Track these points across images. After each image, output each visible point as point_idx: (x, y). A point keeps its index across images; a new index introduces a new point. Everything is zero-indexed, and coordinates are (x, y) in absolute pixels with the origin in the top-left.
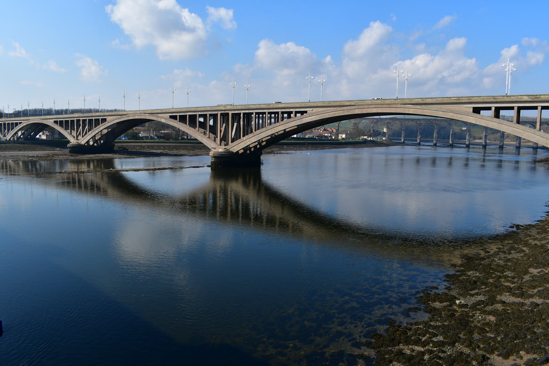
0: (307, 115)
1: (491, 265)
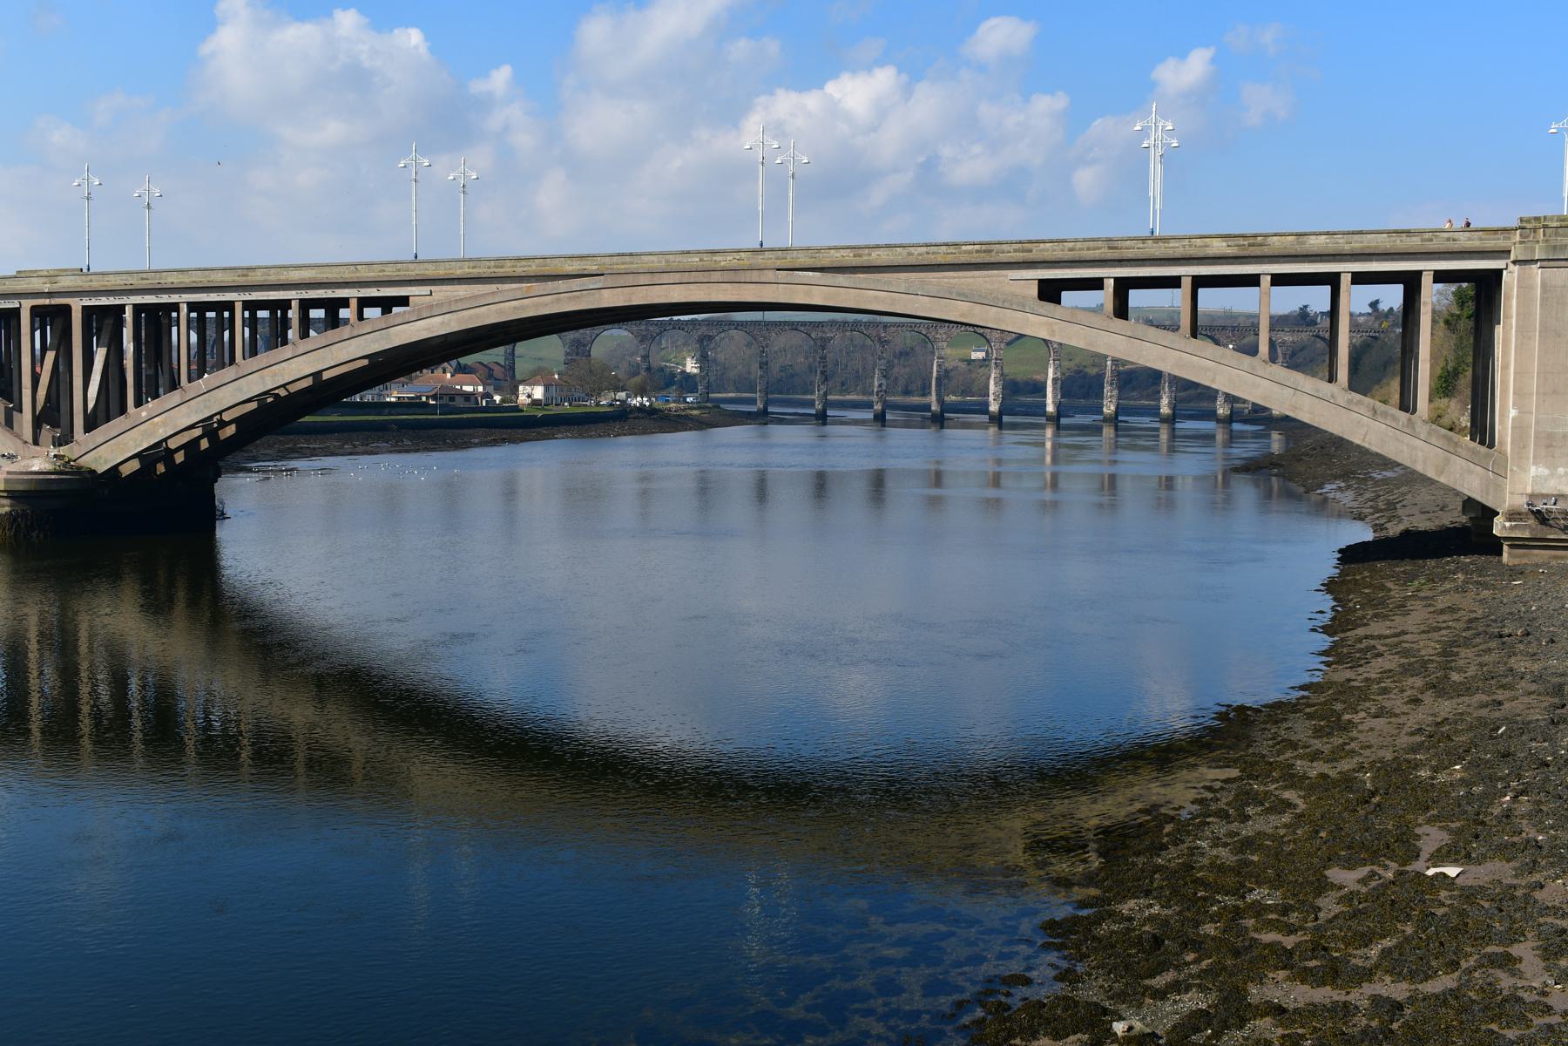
0: (409, 312)
1: (1193, 868)
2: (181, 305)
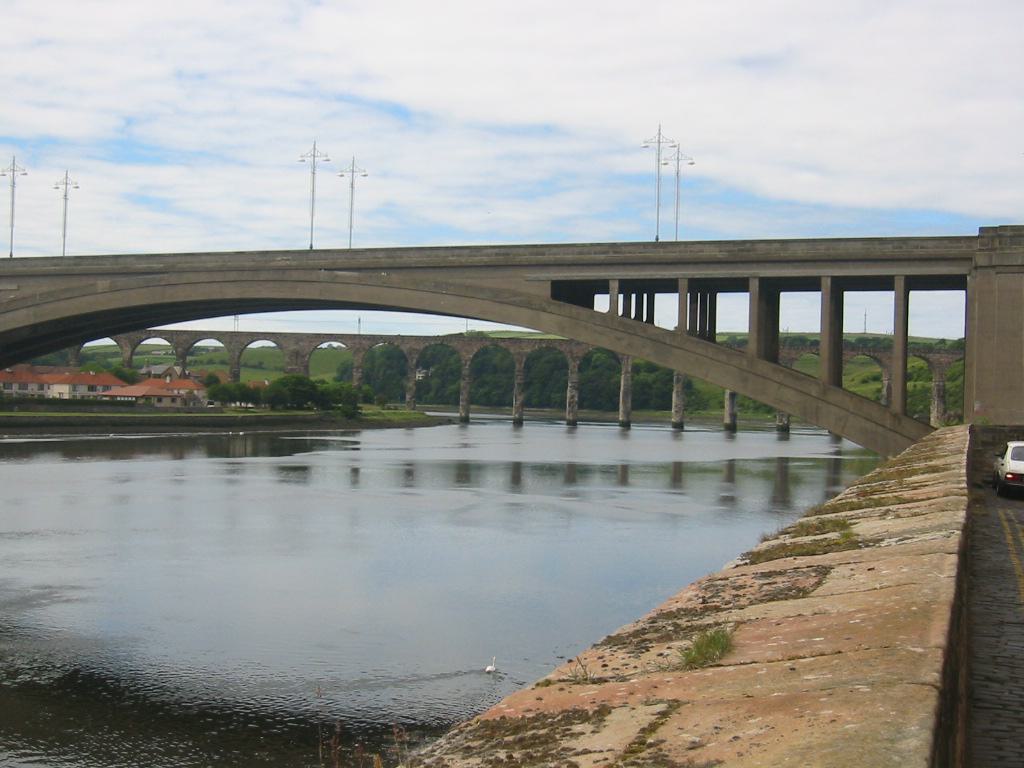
2: (611, 283)
